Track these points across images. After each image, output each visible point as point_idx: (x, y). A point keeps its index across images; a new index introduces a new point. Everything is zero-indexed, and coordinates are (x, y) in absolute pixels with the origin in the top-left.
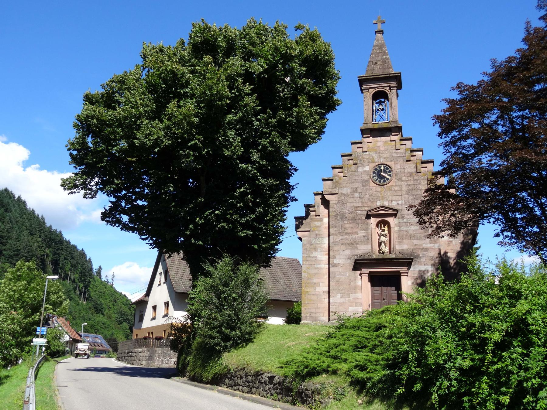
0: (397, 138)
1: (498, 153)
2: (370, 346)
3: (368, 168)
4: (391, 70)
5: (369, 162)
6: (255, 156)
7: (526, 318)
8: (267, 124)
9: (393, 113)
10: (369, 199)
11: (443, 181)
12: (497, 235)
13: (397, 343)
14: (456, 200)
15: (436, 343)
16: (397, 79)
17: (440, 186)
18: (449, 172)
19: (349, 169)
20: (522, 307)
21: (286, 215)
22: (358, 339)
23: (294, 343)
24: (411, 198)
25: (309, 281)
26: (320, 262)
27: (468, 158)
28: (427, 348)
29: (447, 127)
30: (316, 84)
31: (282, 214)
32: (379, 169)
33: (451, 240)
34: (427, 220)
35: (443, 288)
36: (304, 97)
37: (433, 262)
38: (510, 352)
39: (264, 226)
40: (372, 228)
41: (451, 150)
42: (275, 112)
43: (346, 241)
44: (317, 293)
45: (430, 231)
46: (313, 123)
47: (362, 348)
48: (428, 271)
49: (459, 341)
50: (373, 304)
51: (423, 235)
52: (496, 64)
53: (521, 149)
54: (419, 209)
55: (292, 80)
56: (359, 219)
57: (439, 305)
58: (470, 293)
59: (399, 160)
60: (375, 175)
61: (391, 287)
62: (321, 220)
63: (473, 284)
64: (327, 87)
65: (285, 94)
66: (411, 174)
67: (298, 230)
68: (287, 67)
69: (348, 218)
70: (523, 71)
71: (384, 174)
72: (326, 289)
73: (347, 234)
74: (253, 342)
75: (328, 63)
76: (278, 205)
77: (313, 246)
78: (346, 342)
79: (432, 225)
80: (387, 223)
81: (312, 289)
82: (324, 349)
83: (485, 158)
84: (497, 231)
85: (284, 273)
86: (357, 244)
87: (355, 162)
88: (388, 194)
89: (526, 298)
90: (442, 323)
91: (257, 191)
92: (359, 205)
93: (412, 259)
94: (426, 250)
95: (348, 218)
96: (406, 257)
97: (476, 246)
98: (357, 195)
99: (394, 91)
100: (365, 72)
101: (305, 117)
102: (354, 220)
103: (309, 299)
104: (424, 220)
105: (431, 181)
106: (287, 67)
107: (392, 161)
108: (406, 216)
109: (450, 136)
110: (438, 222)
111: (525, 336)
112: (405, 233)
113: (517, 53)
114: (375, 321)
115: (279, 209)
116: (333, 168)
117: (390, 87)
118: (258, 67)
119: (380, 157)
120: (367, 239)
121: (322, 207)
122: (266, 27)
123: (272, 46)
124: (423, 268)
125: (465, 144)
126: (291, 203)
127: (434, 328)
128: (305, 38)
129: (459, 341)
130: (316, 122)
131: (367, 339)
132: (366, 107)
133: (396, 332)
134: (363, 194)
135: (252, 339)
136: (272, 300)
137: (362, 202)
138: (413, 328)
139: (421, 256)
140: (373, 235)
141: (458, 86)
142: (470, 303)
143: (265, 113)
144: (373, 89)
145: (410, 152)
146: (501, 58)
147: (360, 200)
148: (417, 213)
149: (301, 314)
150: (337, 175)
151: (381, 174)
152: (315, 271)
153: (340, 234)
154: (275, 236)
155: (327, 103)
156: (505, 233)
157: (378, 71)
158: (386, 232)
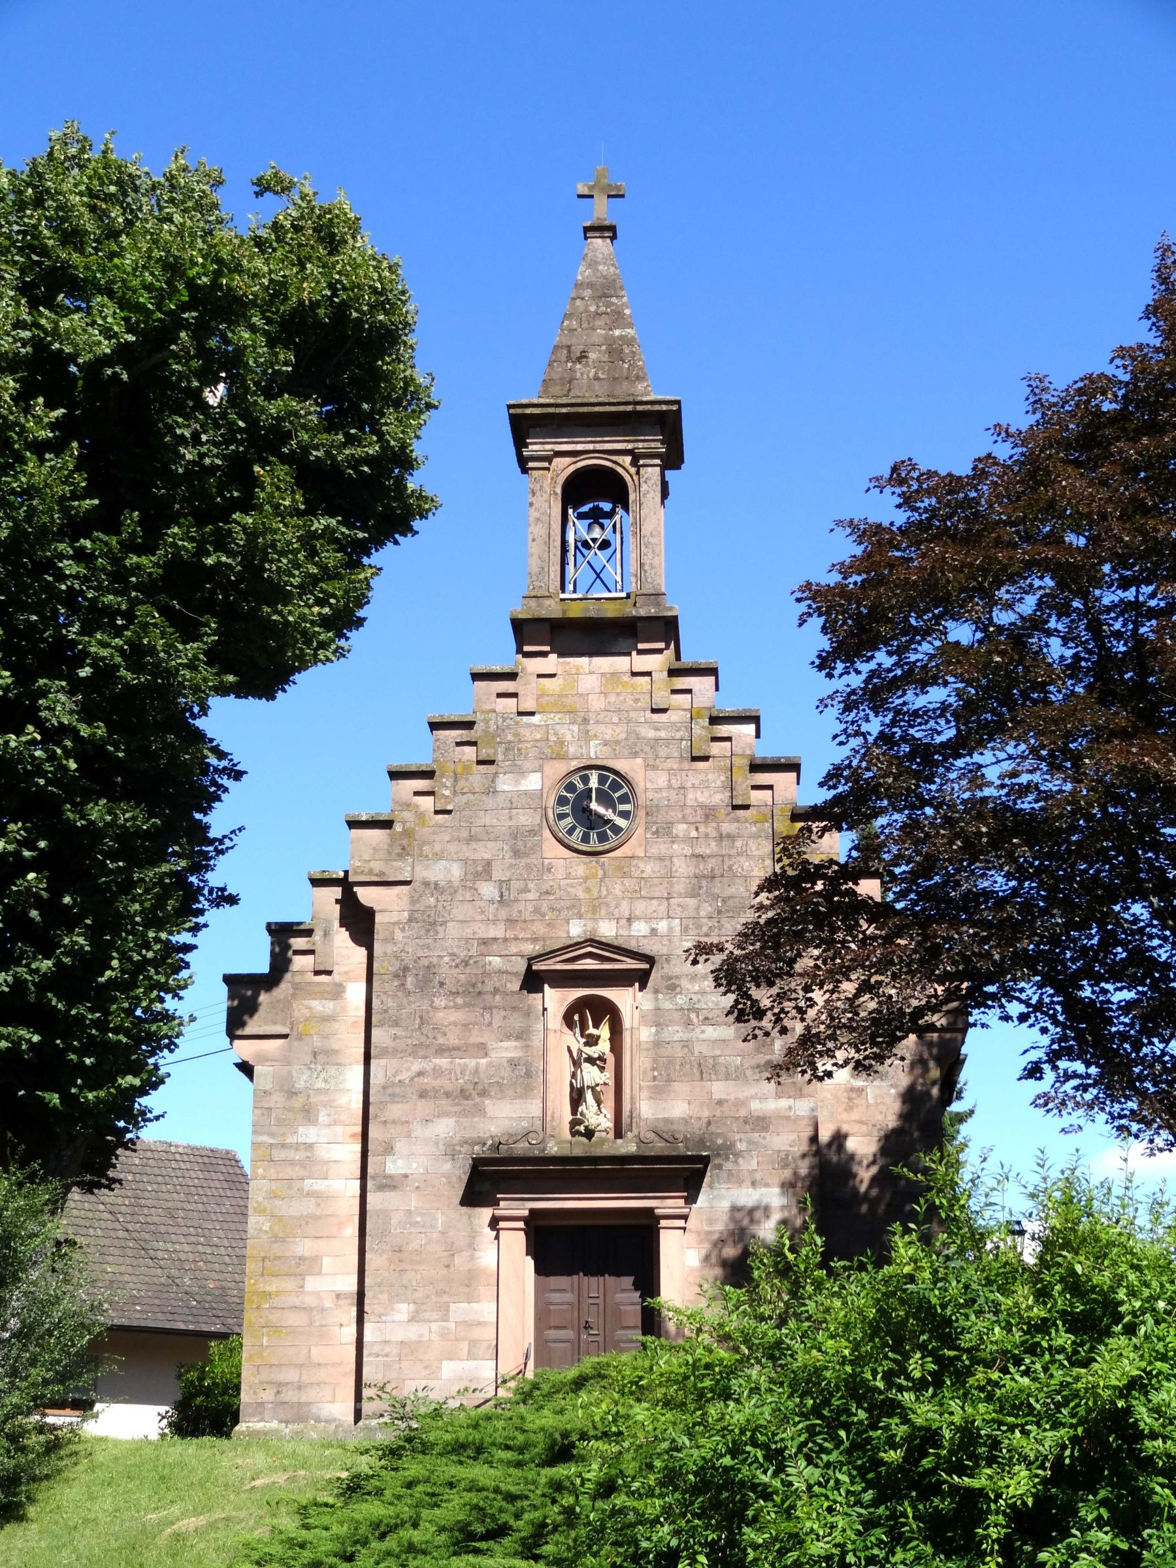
0: (655, 663)
1: (1043, 747)
2: (523, 1527)
3: (536, 782)
4: (640, 386)
5: (544, 758)
6: (60, 706)
7: (1128, 1411)
8: (120, 576)
9: (645, 560)
10: (537, 910)
11: (836, 845)
12: (1033, 1072)
13: (631, 1517)
14: (888, 921)
15: (788, 1513)
16: (664, 426)
17: (819, 867)
18: (857, 811)
19: (462, 783)
20: (1116, 1363)
21: (187, 965)
22: (474, 1498)
23: (202, 1520)
24: (707, 909)
25: (277, 1249)
26: (323, 1170)
27: (927, 758)
28: (749, 1534)
29: (851, 634)
30: (330, 423)
31: (172, 959)
32: (580, 786)
33: (859, 1083)
34: (766, 1003)
35: (818, 1286)
36: (282, 470)
37: (787, 1174)
38: (1069, 1547)
39: (92, 1010)
40: (546, 1029)
41: (865, 727)
42: (156, 521)
43: (437, 1083)
44: (310, 1301)
45: (779, 1045)
46: (315, 580)
47: (489, 1536)
48: (767, 1210)
49: (875, 1503)
50: (543, 1351)
51: (754, 1062)
52: (1045, 397)
53: (1126, 735)
54: (737, 959)
55: (232, 399)
56: (496, 991)
57: (803, 1358)
58: (923, 1310)
59: (663, 752)
60: (567, 809)
61: (618, 1274)
62: (337, 992)
63: (935, 1272)
64: (381, 436)
65: (202, 456)
66: (709, 814)
67: (239, 1032)
68: (213, 343)
69: (450, 985)
70: (1139, 432)
71: (601, 810)
72: (350, 1284)
73: (441, 1051)
74: (22, 1518)
75: (388, 339)
76: (154, 920)
77: (298, 1102)
78: (425, 1513)
79: (786, 1022)
80: (606, 1011)
81: (289, 1284)
82: (330, 1547)
83: (995, 764)
84: (1034, 1056)
85: (171, 1213)
86: (484, 1093)
87: (484, 754)
88: (617, 890)
89: (1130, 1330)
90: (811, 1430)
91: (70, 858)
92: (497, 931)
93: (705, 1161)
94: (761, 1123)
95: (450, 985)
96: (682, 1149)
97: (956, 1107)
98: (488, 890)
99: (652, 473)
100: (539, 387)
101: (282, 553)
102: (474, 992)
103: (276, 1329)
104: (755, 1002)
105: (787, 846)
106: (213, 343)
107: (635, 755)
108: (684, 983)
109: (865, 668)
110: (811, 1013)
111: (1124, 1480)
112: (679, 1053)
113: (1118, 362)
114: (545, 1420)
115: (157, 940)
116: (396, 775)
117: (636, 457)
118: (90, 332)
119: (586, 737)
120: (526, 1077)
121: (342, 937)
122: (132, 169)
123: (156, 254)
124: (747, 1197)
125: (920, 702)
126: (213, 916)
127: (781, 1452)
128: (297, 229)
129: (875, 1503)
130: (328, 574)
131: (511, 1498)
132: (538, 530)
133: (630, 1467)
134: (516, 885)
135: (20, 1505)
136: (115, 1330)
137: (511, 922)
138: (693, 1455)
139: (741, 1146)
140: (551, 1057)
141: (898, 475)
142: (922, 1347)
143: (113, 528)
144: (568, 460)
145: (706, 722)
146: (1063, 378)
147: (503, 913)
148: (728, 977)
149: (237, 1388)
150: (408, 806)
151: (592, 809)
152: (309, 1206)
153: (416, 1051)
154: (134, 1054)
155: (379, 504)
156: (1063, 1064)
157: (590, 387)
158: (604, 1046)
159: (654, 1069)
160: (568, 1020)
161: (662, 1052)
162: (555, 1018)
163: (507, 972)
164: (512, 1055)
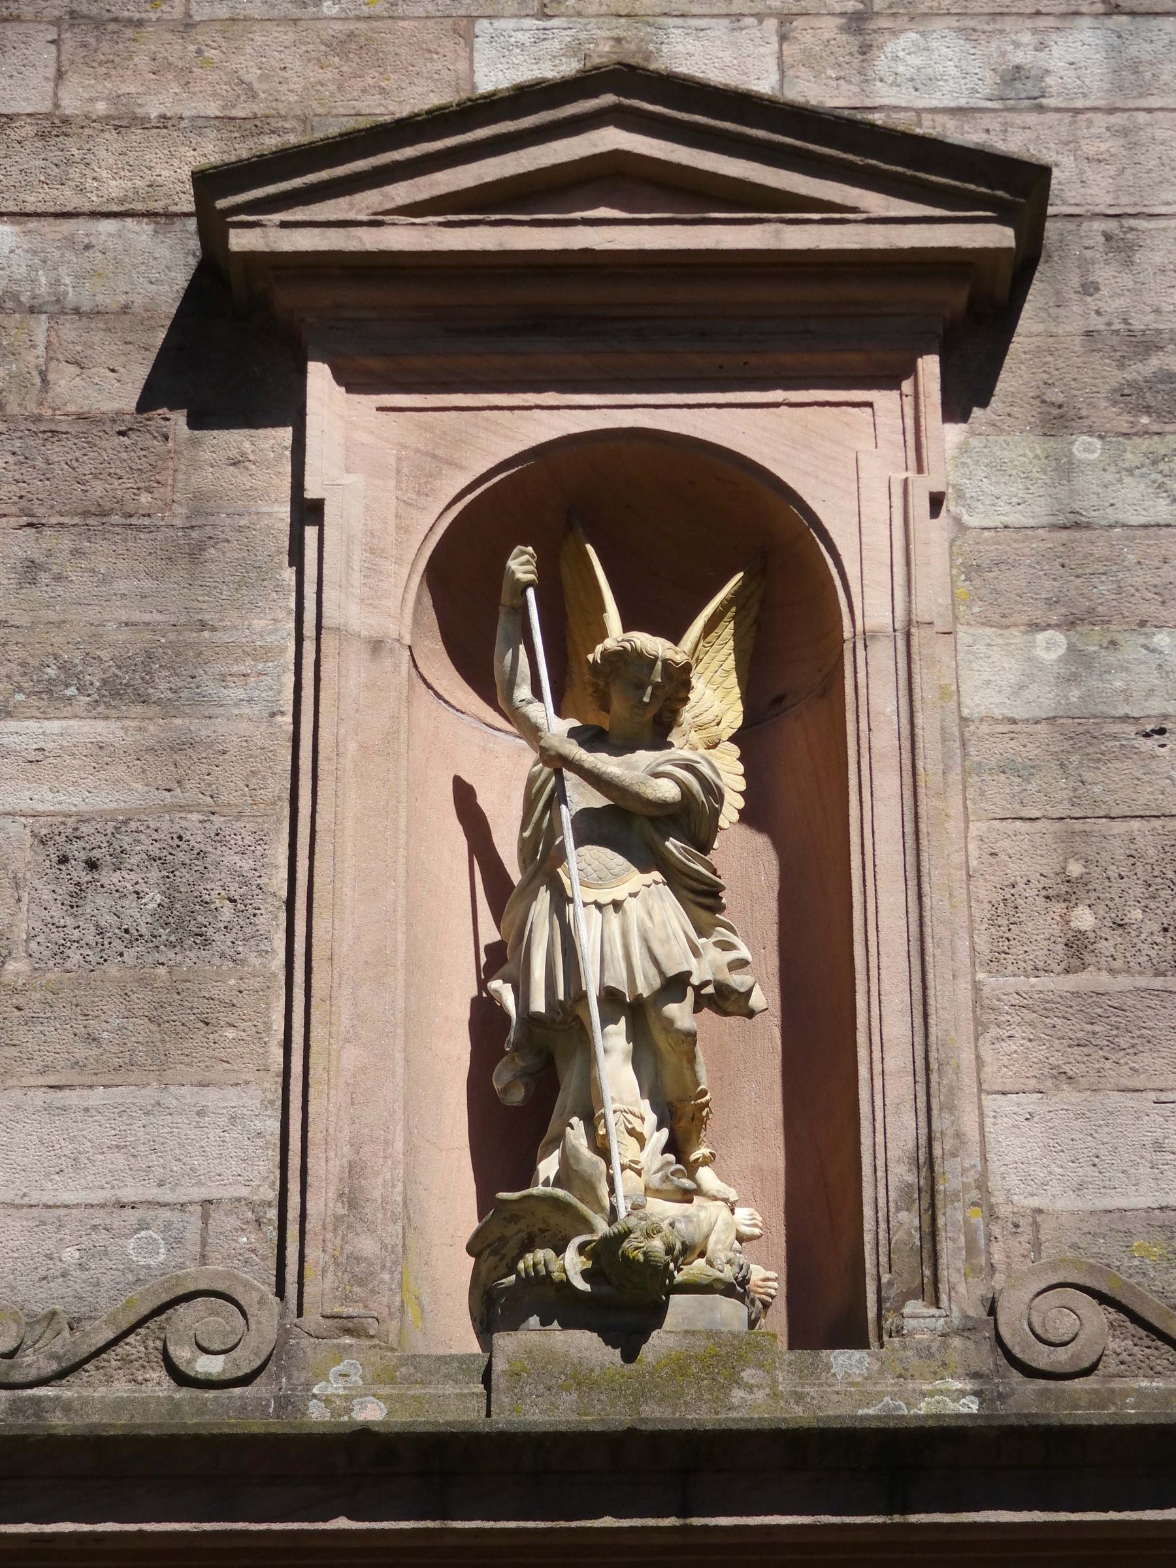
40: (309, 629)
159: (1068, 891)
160: (464, 596)
161: (1113, 782)
162: (377, 582)
163: (59, 309)
164: (75, 801)
